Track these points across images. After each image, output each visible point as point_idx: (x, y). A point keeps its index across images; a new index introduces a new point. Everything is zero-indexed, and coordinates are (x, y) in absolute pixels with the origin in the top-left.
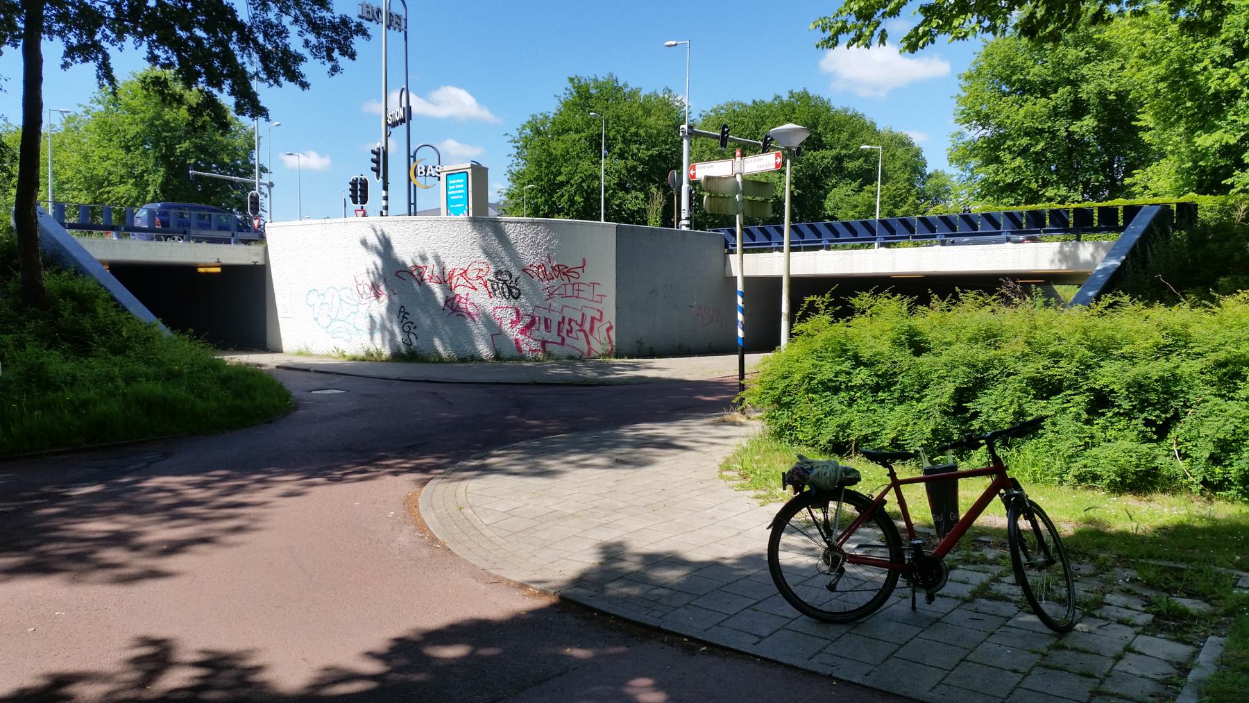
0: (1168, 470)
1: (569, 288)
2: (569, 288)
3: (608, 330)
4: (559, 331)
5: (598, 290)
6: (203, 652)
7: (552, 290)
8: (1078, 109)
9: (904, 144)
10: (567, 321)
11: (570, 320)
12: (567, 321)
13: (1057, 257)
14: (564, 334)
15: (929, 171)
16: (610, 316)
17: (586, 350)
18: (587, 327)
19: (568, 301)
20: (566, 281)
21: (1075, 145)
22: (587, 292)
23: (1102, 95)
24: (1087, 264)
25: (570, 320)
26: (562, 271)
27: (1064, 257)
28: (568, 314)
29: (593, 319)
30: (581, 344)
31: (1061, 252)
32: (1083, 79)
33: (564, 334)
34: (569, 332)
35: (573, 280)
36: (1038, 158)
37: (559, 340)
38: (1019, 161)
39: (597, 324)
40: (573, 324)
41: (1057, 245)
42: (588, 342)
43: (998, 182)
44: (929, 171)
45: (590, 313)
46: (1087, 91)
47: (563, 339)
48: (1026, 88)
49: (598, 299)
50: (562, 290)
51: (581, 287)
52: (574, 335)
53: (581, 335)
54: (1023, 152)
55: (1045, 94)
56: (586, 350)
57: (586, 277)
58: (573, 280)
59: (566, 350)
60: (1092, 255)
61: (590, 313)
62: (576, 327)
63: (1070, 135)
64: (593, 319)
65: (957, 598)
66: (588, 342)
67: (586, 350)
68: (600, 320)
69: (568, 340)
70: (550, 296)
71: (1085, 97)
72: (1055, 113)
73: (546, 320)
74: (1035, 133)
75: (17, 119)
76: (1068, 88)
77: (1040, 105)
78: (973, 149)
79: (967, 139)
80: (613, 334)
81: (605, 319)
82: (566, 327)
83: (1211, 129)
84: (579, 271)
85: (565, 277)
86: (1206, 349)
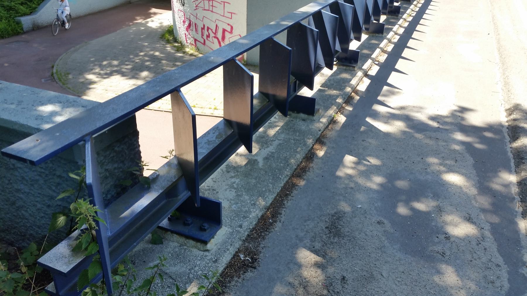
0: (204, 194)
4: (202, 35)
6: (460, 107)
14: (205, 37)
18: (220, 35)
25: (208, 28)
28: (208, 24)
29: (224, 31)
39: (227, 34)
45: (222, 26)
49: (229, 15)
52: (210, 39)
53: (216, 40)
61: (222, 26)
62: (212, 35)
65: (49, 196)
68: (231, 32)
73: (195, 24)
75: (389, 105)
86: (70, 224)
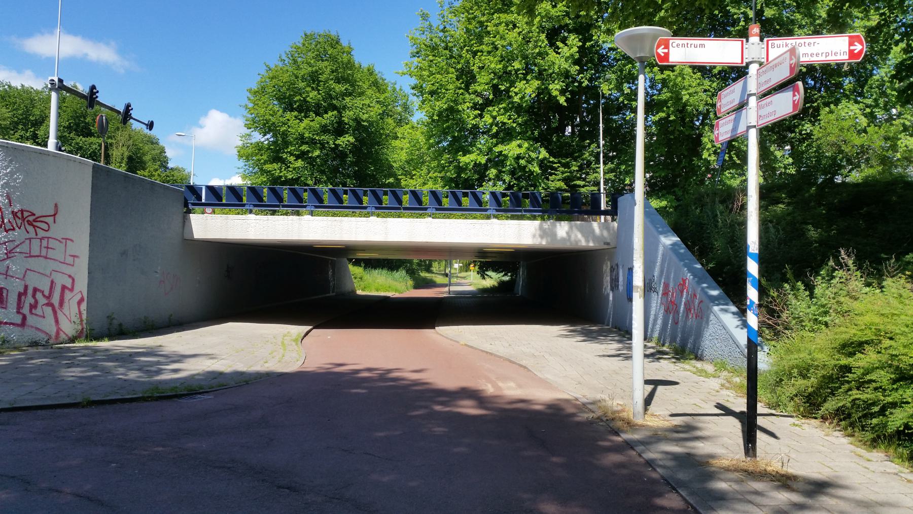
1: (36, 244)
2: (36, 244)
3: (80, 303)
5: (72, 249)
7: (10, 246)
8: (339, 130)
9: (152, 143)
10: (30, 292)
11: (35, 290)
12: (30, 292)
13: (538, 232)
15: (170, 165)
16: (82, 285)
17: (53, 334)
19: (33, 263)
20: (32, 234)
21: (339, 154)
22: (58, 252)
23: (358, 121)
24: (563, 239)
25: (35, 290)
26: (27, 219)
27: (544, 233)
28: (33, 281)
29: (64, 288)
30: (48, 325)
31: (541, 228)
32: (344, 108)
33: (26, 310)
34: (33, 307)
35: (41, 233)
36: (311, 161)
37: (18, 319)
38: (299, 163)
40: (39, 296)
41: (537, 223)
42: (57, 321)
43: (281, 177)
44: (170, 165)
45: (61, 280)
46: (348, 116)
47: (24, 318)
48: (304, 109)
49: (69, 260)
50: (25, 248)
51: (52, 243)
52: (39, 311)
53: (49, 310)
54: (302, 156)
55: (318, 114)
56: (53, 330)
57: (57, 231)
58: (41, 233)
59: (28, 334)
60: (567, 233)
61: (61, 280)
62: (42, 301)
63: (337, 146)
64: (64, 288)
66: (57, 321)
67: (53, 330)
68: (72, 290)
69: (31, 320)
70: (9, 254)
71: (346, 120)
72: (324, 129)
74: (312, 142)
76: (335, 112)
77: (317, 122)
78: (259, 147)
79: (254, 141)
80: (84, 306)
81: (77, 289)
82: (29, 300)
83: (466, 152)
84: (50, 220)
85: (30, 229)
